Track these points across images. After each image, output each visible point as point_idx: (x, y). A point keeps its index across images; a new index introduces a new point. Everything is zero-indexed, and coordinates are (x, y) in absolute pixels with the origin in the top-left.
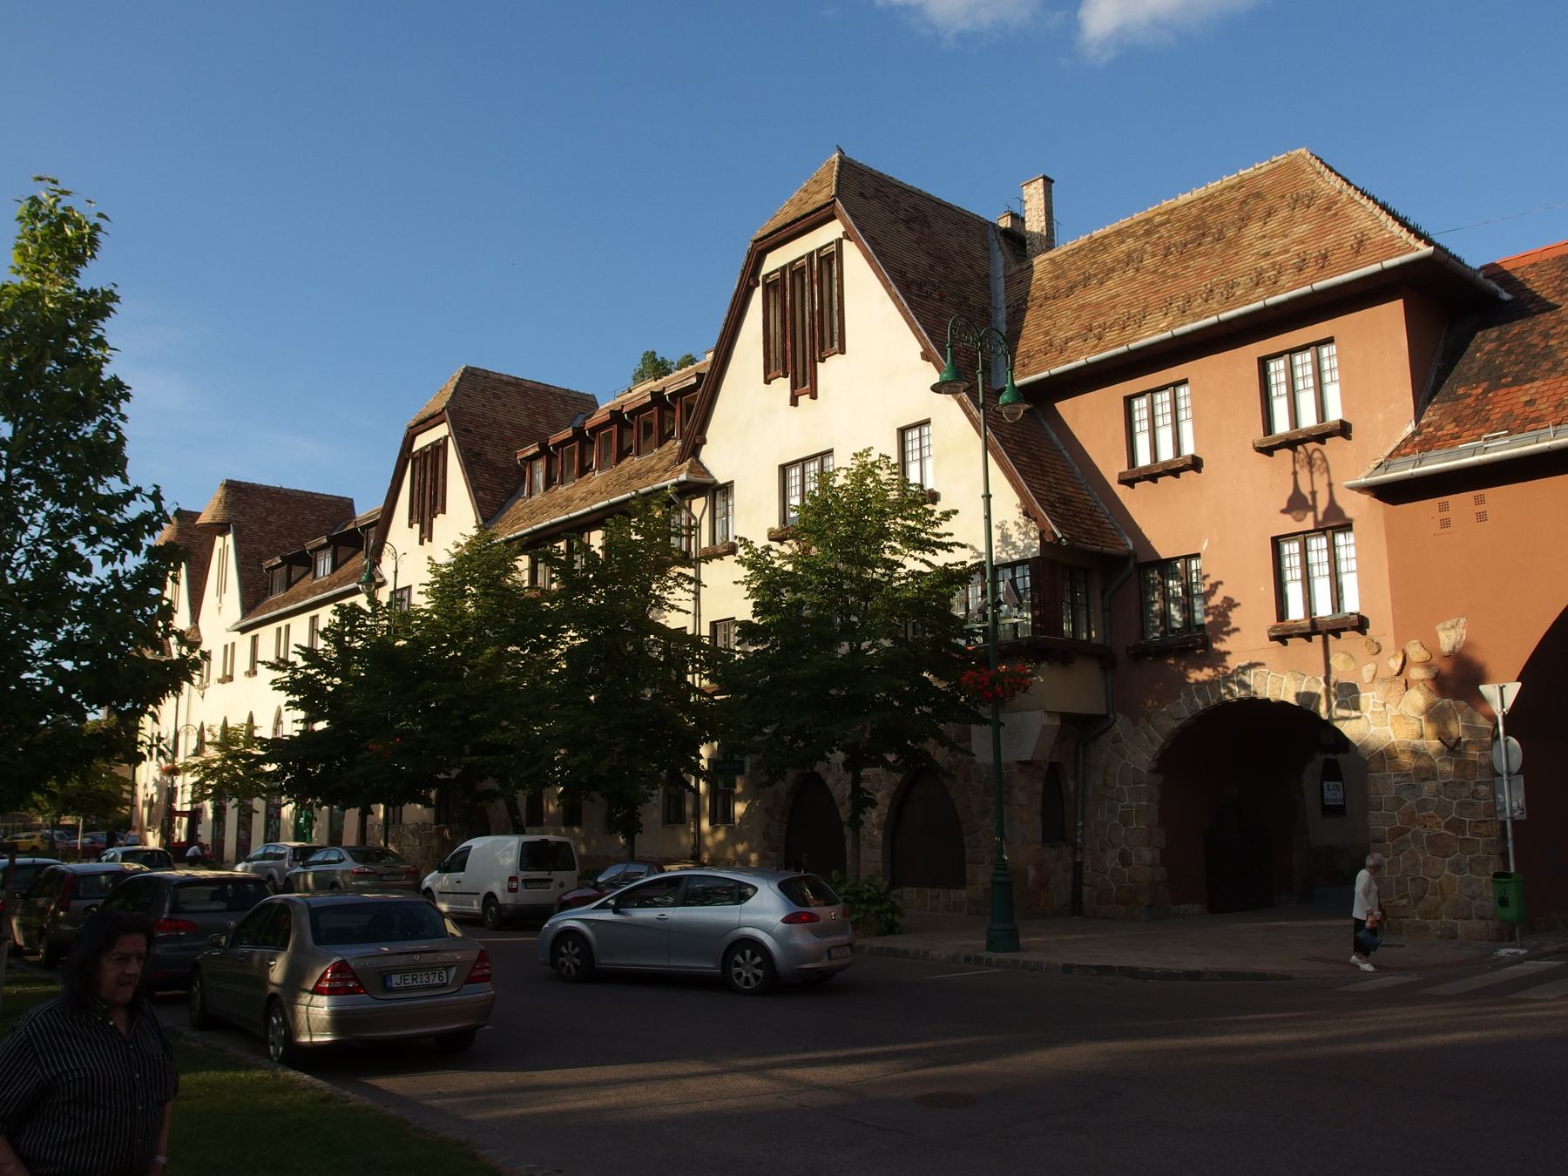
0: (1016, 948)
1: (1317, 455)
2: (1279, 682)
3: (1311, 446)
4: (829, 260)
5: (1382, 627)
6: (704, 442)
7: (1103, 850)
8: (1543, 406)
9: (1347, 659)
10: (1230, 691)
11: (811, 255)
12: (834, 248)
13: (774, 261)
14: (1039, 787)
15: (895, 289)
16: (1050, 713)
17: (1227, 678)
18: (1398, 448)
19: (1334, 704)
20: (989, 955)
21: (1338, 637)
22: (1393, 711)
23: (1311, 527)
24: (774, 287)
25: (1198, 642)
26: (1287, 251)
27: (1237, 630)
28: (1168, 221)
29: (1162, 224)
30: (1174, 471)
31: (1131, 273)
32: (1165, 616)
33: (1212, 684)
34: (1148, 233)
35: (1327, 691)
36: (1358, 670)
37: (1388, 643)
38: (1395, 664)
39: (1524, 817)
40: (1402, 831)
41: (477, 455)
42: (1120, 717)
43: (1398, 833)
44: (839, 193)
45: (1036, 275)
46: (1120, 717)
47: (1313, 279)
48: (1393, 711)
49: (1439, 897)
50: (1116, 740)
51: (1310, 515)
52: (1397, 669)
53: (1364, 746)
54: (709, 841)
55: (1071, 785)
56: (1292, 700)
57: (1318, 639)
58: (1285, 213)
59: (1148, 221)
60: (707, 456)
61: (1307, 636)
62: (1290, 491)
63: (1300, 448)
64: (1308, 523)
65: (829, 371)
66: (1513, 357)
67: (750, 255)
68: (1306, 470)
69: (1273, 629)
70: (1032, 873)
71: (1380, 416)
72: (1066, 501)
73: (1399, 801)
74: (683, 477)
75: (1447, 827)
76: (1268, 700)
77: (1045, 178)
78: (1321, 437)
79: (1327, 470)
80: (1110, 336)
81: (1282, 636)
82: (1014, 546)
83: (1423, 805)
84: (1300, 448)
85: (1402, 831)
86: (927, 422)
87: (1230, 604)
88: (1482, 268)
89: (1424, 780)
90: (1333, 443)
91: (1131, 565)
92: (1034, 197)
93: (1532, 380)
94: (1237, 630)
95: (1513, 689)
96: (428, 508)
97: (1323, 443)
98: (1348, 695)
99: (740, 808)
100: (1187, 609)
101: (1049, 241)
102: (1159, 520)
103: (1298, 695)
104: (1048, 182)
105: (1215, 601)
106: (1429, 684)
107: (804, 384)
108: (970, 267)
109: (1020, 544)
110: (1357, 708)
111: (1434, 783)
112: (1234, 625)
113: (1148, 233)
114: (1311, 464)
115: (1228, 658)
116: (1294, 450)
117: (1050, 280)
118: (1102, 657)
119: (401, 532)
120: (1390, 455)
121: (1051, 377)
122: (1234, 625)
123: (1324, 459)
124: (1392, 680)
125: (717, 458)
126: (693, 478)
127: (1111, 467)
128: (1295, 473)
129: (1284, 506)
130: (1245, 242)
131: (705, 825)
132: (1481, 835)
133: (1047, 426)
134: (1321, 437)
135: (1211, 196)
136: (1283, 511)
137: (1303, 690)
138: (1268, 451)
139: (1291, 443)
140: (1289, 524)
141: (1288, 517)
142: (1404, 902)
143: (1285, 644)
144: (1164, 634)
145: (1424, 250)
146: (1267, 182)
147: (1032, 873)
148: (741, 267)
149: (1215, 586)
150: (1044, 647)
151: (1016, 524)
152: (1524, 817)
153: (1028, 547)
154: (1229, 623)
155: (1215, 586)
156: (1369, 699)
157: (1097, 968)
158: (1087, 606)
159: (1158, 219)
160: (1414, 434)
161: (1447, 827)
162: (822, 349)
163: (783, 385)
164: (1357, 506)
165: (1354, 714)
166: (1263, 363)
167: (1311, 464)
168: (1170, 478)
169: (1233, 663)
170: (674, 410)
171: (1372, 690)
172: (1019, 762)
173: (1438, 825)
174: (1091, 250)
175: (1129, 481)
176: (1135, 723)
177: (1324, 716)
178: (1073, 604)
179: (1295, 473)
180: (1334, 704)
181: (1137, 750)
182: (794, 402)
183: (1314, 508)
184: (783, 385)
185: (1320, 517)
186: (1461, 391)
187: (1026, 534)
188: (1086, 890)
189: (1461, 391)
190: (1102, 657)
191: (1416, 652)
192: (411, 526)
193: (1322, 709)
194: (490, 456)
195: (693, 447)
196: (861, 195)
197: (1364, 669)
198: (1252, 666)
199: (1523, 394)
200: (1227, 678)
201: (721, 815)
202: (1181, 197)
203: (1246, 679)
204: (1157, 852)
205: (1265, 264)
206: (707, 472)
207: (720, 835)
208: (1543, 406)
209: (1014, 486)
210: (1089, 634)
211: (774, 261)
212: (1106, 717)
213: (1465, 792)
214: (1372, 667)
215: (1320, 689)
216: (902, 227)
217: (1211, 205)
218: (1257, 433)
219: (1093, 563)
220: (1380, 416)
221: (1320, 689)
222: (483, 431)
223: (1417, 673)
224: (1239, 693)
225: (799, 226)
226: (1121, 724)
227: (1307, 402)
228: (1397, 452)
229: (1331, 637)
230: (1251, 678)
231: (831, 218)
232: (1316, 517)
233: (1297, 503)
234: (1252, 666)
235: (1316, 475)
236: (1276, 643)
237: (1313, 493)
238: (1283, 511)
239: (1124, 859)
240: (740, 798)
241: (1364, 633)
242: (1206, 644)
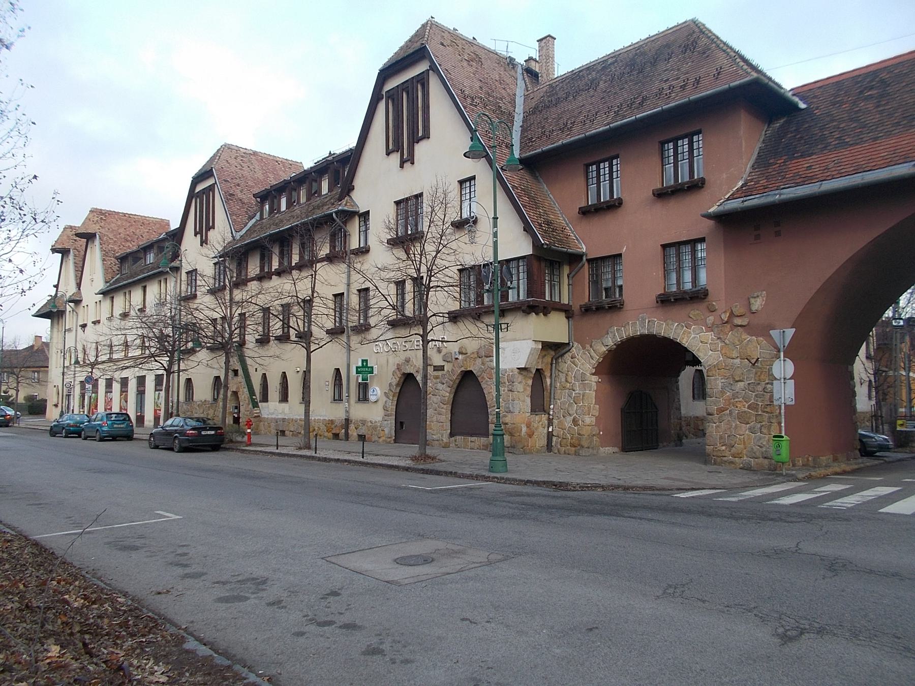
8: (816, 169)
14: (530, 382)
24: (394, 96)
26: (678, 79)
28: (616, 61)
29: (613, 63)
39: (793, 403)
41: (231, 195)
42: (576, 344)
43: (721, 410)
46: (576, 344)
49: (742, 446)
55: (548, 381)
60: (356, 195)
65: (421, 149)
66: (803, 141)
70: (524, 429)
71: (724, 176)
75: (749, 408)
86: (474, 178)
88: (792, 90)
91: (584, 259)
93: (812, 154)
95: (790, 332)
96: (204, 228)
107: (408, 159)
119: (190, 242)
125: (361, 198)
132: (767, 412)
142: (724, 448)
145: (755, 75)
147: (524, 429)
152: (793, 403)
159: (610, 61)
161: (749, 408)
163: (395, 158)
176: (584, 348)
178: (550, 281)
182: (402, 166)
184: (395, 158)
186: (771, 161)
189: (771, 161)
192: (196, 235)
194: (240, 195)
196: (442, 44)
199: (805, 163)
204: (594, 419)
205: (665, 86)
208: (816, 169)
212: (569, 344)
213: (760, 388)
216: (465, 64)
220: (724, 176)
222: (237, 181)
226: (576, 349)
227: (684, 166)
231: (529, 293)
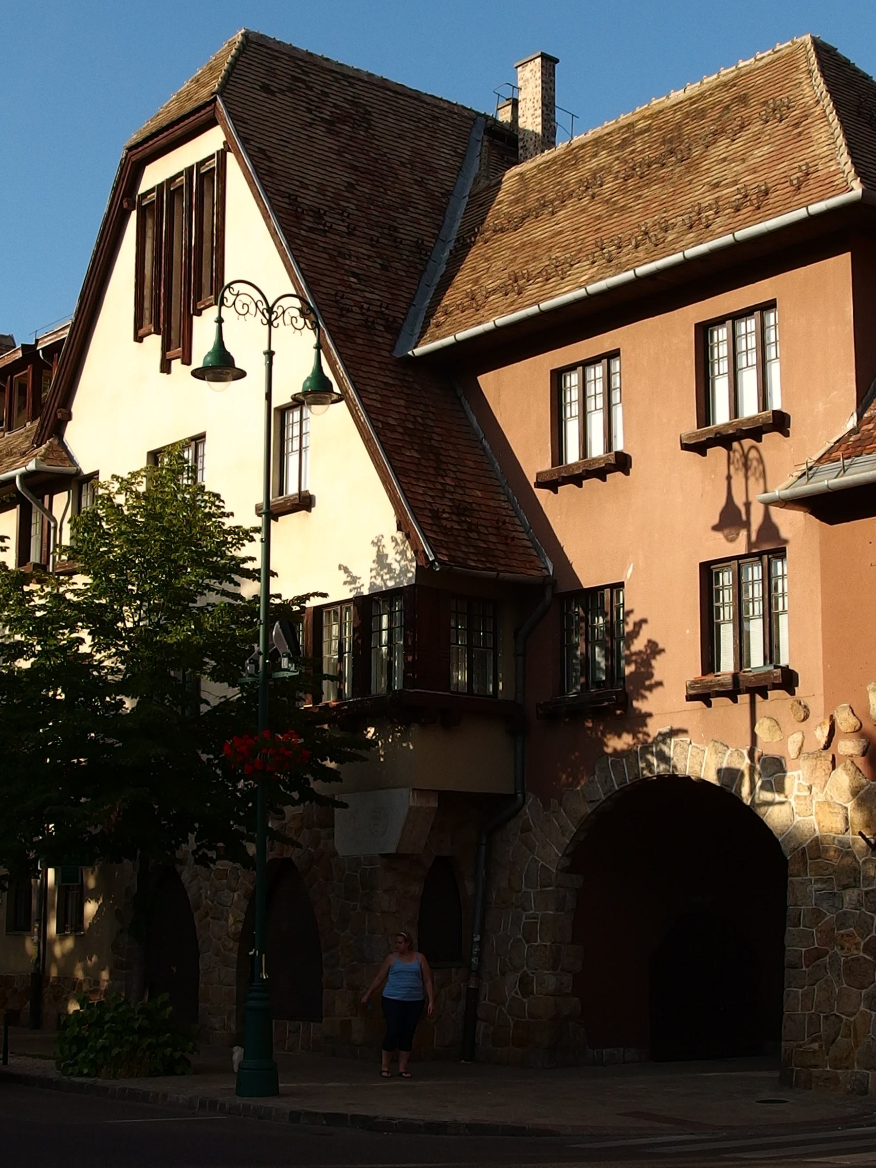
0: (275, 1092)
1: (753, 454)
2: (700, 756)
3: (747, 442)
4: (208, 179)
5: (811, 686)
6: (69, 417)
7: (503, 974)
9: (781, 729)
10: (649, 766)
11: (189, 170)
12: (214, 163)
13: (154, 176)
14: (416, 889)
15: (274, 222)
16: (421, 792)
17: (646, 748)
18: (830, 451)
19: (759, 783)
20: (240, 1101)
21: (765, 697)
22: (819, 796)
23: (743, 551)
25: (617, 698)
27: (660, 684)
28: (648, 129)
30: (601, 473)
31: (585, 201)
32: (588, 662)
33: (628, 754)
34: (625, 143)
35: (752, 769)
36: (783, 742)
37: (817, 707)
38: (821, 735)
40: (819, 954)
42: (531, 799)
44: (222, 90)
45: (501, 196)
47: (745, 224)
48: (819, 796)
49: (852, 1041)
50: (526, 829)
51: (743, 533)
52: (823, 740)
53: (791, 836)
54: (58, 950)
56: (711, 777)
57: (744, 699)
58: (754, 128)
59: (631, 125)
60: (75, 436)
61: (732, 695)
62: (722, 502)
63: (735, 445)
64: (740, 547)
67: (123, 167)
68: (741, 474)
69: (692, 685)
72: (460, 510)
73: (818, 914)
74: (32, 466)
76: (689, 777)
77: (544, 56)
78: (756, 432)
79: (764, 474)
80: (532, 289)
81: (702, 695)
82: (390, 570)
83: (842, 920)
84: (735, 445)
85: (819, 954)
87: (654, 649)
89: (845, 887)
90: (771, 439)
92: (530, 80)
94: (660, 684)
97: (759, 440)
98: (773, 771)
99: (91, 908)
100: (612, 654)
101: (548, 138)
102: (589, 537)
103: (719, 771)
104: (549, 63)
105: (638, 645)
106: (860, 762)
108: (420, 183)
109: (396, 566)
110: (781, 789)
111: (856, 891)
112: (657, 677)
113: (625, 143)
114: (746, 466)
115: (649, 721)
116: (729, 448)
117: (511, 203)
118: (509, 717)
120: (819, 460)
121: (458, 344)
122: (657, 677)
123: (761, 460)
124: (816, 756)
126: (44, 466)
127: (534, 461)
128: (729, 478)
129: (716, 520)
130: (705, 166)
131: (52, 928)
133: (467, 406)
134: (756, 432)
135: (702, 96)
136: (715, 528)
137: (724, 765)
138: (699, 448)
139: (724, 439)
140: (722, 547)
141: (719, 536)
142: (816, 1046)
143: (709, 705)
144: (585, 686)
146: (760, 81)
148: (111, 183)
149: (639, 624)
150: (423, 705)
151: (394, 539)
153: (404, 571)
154: (651, 675)
155: (639, 624)
156: (795, 779)
157: (326, 1116)
158: (495, 650)
159: (641, 125)
160: (852, 432)
162: (198, 298)
164: (792, 524)
165: (778, 798)
166: (704, 331)
167: (746, 466)
168: (595, 481)
169: (654, 728)
170: (51, 369)
171: (798, 768)
172: (383, 856)
173: (857, 944)
174: (562, 165)
175: (551, 484)
177: (747, 801)
179: (729, 478)
180: (759, 783)
181: (546, 841)
183: (747, 525)
185: (754, 537)
187: (403, 553)
188: (481, 1027)
190: (509, 717)
191: (845, 721)
193: (745, 790)
195: (55, 420)
196: (265, 88)
197: (790, 739)
198: (673, 733)
200: (646, 748)
201: (71, 921)
202: (673, 95)
203: (665, 749)
206: (70, 458)
207: (69, 943)
209: (387, 490)
210: (496, 686)
211: (154, 176)
214: (797, 737)
215: (744, 764)
216: (320, 131)
217: (695, 110)
218: (689, 425)
219: (492, 588)
220: (820, 407)
221: (744, 764)
223: (848, 747)
224: (660, 768)
225: (178, 131)
228: (827, 457)
229: (758, 698)
230: (671, 749)
231: (211, 123)
232: (749, 536)
233: (731, 519)
234: (673, 733)
235: (752, 480)
236: (699, 704)
237: (748, 505)
238: (715, 528)
239: (525, 984)
240: (93, 895)
241: (792, 693)
242: (625, 702)
